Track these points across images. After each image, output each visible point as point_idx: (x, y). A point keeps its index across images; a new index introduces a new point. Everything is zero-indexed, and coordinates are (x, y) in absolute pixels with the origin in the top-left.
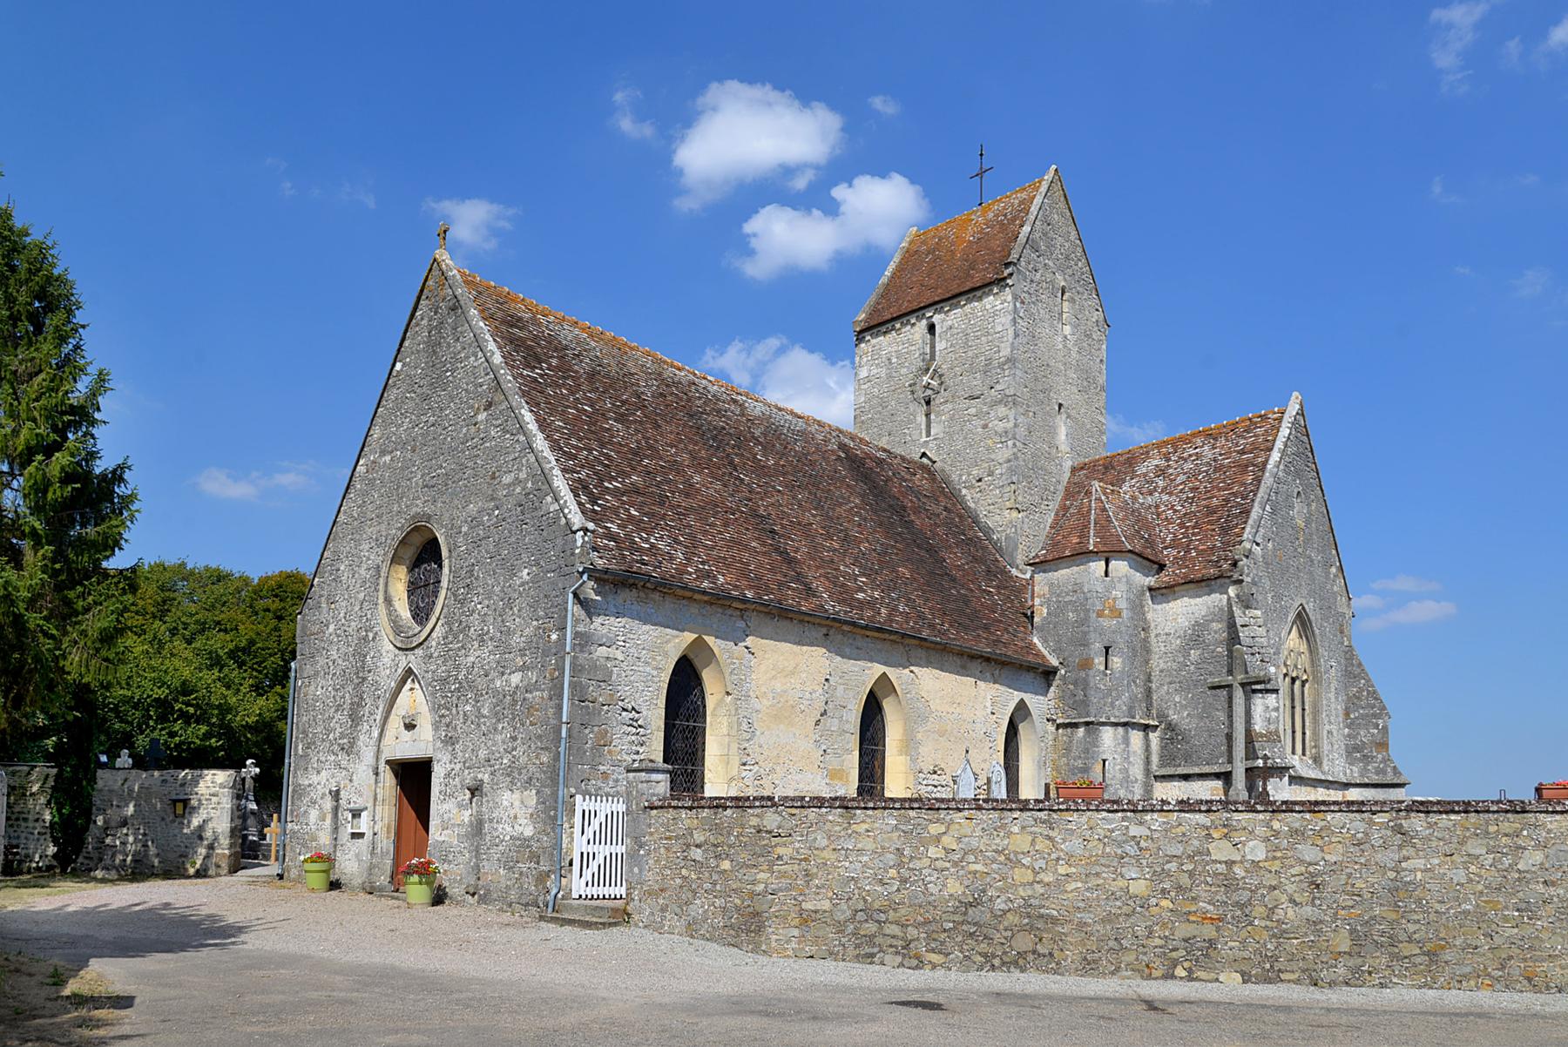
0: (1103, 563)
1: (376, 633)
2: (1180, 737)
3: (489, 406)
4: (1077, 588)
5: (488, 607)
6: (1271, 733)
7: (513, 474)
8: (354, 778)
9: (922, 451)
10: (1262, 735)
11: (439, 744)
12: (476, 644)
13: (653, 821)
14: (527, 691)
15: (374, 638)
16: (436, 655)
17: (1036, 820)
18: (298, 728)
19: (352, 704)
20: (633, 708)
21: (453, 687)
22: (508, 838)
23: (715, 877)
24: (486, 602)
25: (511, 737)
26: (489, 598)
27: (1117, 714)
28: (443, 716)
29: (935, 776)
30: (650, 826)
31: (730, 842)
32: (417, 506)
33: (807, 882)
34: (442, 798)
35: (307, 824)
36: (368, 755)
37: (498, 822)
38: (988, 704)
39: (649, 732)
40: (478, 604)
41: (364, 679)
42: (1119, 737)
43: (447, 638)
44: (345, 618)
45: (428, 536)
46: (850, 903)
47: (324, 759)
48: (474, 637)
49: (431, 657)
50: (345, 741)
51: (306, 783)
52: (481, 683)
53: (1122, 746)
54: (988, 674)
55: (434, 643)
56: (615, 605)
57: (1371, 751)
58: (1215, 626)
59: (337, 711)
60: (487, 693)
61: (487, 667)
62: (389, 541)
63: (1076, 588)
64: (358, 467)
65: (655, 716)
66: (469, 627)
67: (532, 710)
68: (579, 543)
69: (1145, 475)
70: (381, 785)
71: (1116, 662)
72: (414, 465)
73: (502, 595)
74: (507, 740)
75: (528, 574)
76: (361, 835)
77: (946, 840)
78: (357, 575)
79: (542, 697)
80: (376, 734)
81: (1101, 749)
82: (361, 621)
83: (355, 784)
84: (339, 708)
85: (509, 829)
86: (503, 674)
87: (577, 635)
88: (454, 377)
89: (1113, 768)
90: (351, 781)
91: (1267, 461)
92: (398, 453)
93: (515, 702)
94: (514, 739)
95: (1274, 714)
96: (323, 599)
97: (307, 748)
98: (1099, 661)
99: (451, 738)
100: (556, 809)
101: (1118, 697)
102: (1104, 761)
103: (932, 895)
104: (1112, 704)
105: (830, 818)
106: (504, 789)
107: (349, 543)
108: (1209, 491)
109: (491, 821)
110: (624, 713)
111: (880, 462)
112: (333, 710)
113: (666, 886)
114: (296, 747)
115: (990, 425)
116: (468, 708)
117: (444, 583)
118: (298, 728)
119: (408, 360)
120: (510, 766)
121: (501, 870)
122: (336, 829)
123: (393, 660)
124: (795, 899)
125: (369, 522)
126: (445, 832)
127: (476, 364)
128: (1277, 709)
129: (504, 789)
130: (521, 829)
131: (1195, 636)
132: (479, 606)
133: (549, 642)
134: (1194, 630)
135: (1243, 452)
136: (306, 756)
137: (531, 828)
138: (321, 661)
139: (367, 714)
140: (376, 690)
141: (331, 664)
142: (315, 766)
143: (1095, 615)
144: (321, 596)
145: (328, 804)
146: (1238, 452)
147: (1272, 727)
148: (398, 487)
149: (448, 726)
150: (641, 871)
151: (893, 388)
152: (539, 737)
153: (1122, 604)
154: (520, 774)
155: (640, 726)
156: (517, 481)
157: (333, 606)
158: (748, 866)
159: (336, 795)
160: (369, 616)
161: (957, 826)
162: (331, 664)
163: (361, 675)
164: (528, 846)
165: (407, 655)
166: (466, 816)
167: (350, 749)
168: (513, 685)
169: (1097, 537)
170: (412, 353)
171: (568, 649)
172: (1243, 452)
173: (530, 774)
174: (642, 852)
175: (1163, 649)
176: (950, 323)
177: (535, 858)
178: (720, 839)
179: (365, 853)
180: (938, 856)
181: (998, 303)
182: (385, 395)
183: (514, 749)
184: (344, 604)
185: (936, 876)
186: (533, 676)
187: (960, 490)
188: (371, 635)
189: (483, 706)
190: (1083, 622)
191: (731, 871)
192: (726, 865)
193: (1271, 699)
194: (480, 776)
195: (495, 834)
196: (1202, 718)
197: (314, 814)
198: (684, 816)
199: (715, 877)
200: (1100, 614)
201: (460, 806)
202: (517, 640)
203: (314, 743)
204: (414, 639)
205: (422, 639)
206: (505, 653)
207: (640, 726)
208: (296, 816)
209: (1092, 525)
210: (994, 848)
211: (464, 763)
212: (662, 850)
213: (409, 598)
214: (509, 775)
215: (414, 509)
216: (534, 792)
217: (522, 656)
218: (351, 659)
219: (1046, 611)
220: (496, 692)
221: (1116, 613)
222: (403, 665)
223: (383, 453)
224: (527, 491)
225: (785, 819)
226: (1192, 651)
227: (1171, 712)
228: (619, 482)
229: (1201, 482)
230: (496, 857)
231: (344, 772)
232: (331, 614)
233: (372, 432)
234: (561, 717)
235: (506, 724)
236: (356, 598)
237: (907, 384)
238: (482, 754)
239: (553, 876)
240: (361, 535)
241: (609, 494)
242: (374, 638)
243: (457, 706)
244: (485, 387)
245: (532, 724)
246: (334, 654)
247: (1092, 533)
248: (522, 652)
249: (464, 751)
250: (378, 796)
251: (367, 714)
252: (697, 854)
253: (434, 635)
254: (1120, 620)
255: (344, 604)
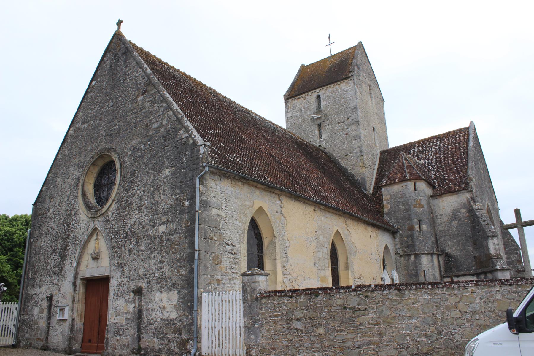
0: (413, 183)
1: (77, 211)
2: (453, 259)
3: (144, 92)
4: (403, 196)
5: (144, 191)
6: (498, 254)
7: (158, 123)
8: (61, 289)
9: (319, 144)
10: (494, 256)
11: (113, 267)
12: (137, 212)
13: (263, 306)
14: (170, 235)
15: (75, 214)
16: (112, 219)
17: (509, 291)
18: (30, 264)
19: (61, 249)
20: (231, 243)
21: (122, 236)
22: (159, 320)
23: (313, 339)
24: (143, 189)
25: (160, 261)
26: (145, 187)
27: (428, 250)
28: (116, 252)
29: (360, 280)
30: (261, 309)
31: (322, 316)
32: (102, 145)
33: (380, 338)
34: (115, 298)
35: (32, 316)
36: (70, 276)
37: (152, 310)
38: (376, 246)
39: (239, 257)
40: (138, 190)
41: (69, 235)
42: (430, 260)
43: (119, 210)
44: (59, 205)
45: (107, 160)
46: (409, 350)
47: (43, 279)
48: (135, 208)
49: (109, 220)
50: (57, 269)
51: (33, 293)
52: (140, 233)
53: (431, 264)
54: (374, 232)
55: (111, 214)
56: (220, 187)
57: (516, 264)
58: (463, 211)
59: (52, 253)
60: (144, 238)
61: (143, 224)
62: (85, 165)
63: (403, 195)
64: (70, 132)
65: (242, 249)
66: (132, 203)
67: (173, 245)
68: (202, 152)
69: (414, 153)
70: (77, 292)
71: (424, 227)
72: (101, 126)
73: (152, 184)
74: (157, 263)
75: (169, 171)
76: (64, 320)
77: (461, 306)
78: (66, 183)
79: (180, 238)
80: (75, 264)
81: (423, 265)
82: (68, 206)
83: (62, 292)
84: (54, 252)
85: (160, 314)
86: (154, 226)
87: (202, 202)
88: (124, 83)
89: (429, 274)
90: (59, 290)
91: (468, 145)
92: (92, 122)
93: (162, 241)
94: (162, 262)
95: (497, 247)
96: (47, 197)
97: (35, 274)
98: (417, 227)
99: (121, 264)
100: (192, 301)
101: (427, 243)
102: (424, 271)
103: (457, 341)
104: (425, 245)
105: (390, 297)
106: (156, 291)
107: (62, 168)
108: (445, 158)
109: (147, 310)
110: (227, 246)
111: (307, 146)
112: (50, 253)
113: (276, 346)
114: (28, 273)
115: (349, 133)
116: (132, 246)
117: (118, 181)
118: (30, 264)
119: (99, 79)
120: (159, 278)
121: (155, 340)
122: (49, 318)
123: (86, 224)
124: (374, 350)
125: (74, 157)
126: (118, 317)
127: (137, 75)
128: (498, 244)
129: (156, 291)
130: (168, 314)
131: (454, 216)
132: (138, 192)
133: (184, 206)
134: (453, 213)
135: (455, 143)
136: (33, 278)
137: (175, 313)
138: (45, 228)
139: (70, 254)
140: (75, 241)
141: (50, 229)
142: (39, 283)
143: (413, 207)
144: (46, 195)
145: (45, 304)
146: (453, 143)
147: (498, 252)
148: (91, 138)
149: (119, 257)
150: (256, 337)
151: (303, 120)
152: (179, 260)
153: (424, 202)
154: (166, 281)
155: (235, 253)
156: (162, 126)
157: (52, 200)
158: (337, 331)
159: (50, 299)
160: (73, 203)
161: (465, 297)
162: (50, 229)
163: (67, 233)
164: (173, 324)
165: (94, 221)
166: (131, 308)
167: (60, 273)
168: (161, 232)
169: (409, 174)
170: (101, 76)
171: (197, 209)
172: (455, 143)
173: (173, 282)
174: (256, 326)
175: (440, 221)
176: (327, 94)
177: (178, 331)
178: (314, 314)
179: (67, 331)
180: (458, 316)
181: (347, 86)
182: (86, 97)
183: (162, 268)
184: (58, 198)
185: (458, 329)
186: (173, 226)
187: (338, 160)
188: (73, 213)
189: (141, 245)
190: (408, 210)
191: (325, 335)
192: (321, 331)
193: (495, 240)
194: (140, 284)
195: (150, 318)
196: (462, 250)
197: (36, 310)
198: (286, 302)
199: (313, 339)
200: (415, 206)
201: (127, 302)
202: (163, 207)
203: (39, 271)
204: (99, 212)
205: (103, 212)
206: (155, 215)
207: (235, 253)
208: (26, 311)
209: (406, 169)
210: (489, 309)
211: (130, 277)
212: (271, 324)
213: (95, 193)
214: (159, 283)
215: (100, 147)
216: (176, 292)
217: (166, 215)
218: (62, 225)
219: (389, 206)
220: (149, 236)
221: (422, 206)
222: (92, 225)
223: (83, 123)
224: (167, 129)
225: (362, 299)
226: (454, 222)
227: (447, 248)
228: (212, 131)
229: (441, 155)
230: (151, 331)
231: (56, 286)
232: (51, 204)
233: (78, 114)
234: (194, 248)
235: (156, 254)
236: (65, 195)
237: (309, 119)
238: (141, 272)
239: (191, 342)
240: (70, 163)
241: (210, 135)
242: (75, 214)
243: (125, 246)
244: (142, 85)
245: (173, 253)
246: (52, 224)
247: (407, 173)
248: (166, 214)
249: (129, 271)
250: (76, 298)
251: (70, 254)
252: (298, 325)
253: (111, 209)
254: (424, 209)
255: (58, 198)
